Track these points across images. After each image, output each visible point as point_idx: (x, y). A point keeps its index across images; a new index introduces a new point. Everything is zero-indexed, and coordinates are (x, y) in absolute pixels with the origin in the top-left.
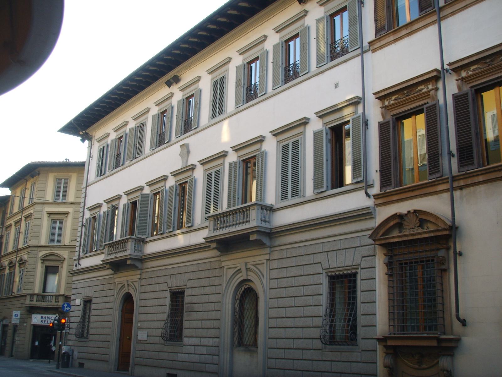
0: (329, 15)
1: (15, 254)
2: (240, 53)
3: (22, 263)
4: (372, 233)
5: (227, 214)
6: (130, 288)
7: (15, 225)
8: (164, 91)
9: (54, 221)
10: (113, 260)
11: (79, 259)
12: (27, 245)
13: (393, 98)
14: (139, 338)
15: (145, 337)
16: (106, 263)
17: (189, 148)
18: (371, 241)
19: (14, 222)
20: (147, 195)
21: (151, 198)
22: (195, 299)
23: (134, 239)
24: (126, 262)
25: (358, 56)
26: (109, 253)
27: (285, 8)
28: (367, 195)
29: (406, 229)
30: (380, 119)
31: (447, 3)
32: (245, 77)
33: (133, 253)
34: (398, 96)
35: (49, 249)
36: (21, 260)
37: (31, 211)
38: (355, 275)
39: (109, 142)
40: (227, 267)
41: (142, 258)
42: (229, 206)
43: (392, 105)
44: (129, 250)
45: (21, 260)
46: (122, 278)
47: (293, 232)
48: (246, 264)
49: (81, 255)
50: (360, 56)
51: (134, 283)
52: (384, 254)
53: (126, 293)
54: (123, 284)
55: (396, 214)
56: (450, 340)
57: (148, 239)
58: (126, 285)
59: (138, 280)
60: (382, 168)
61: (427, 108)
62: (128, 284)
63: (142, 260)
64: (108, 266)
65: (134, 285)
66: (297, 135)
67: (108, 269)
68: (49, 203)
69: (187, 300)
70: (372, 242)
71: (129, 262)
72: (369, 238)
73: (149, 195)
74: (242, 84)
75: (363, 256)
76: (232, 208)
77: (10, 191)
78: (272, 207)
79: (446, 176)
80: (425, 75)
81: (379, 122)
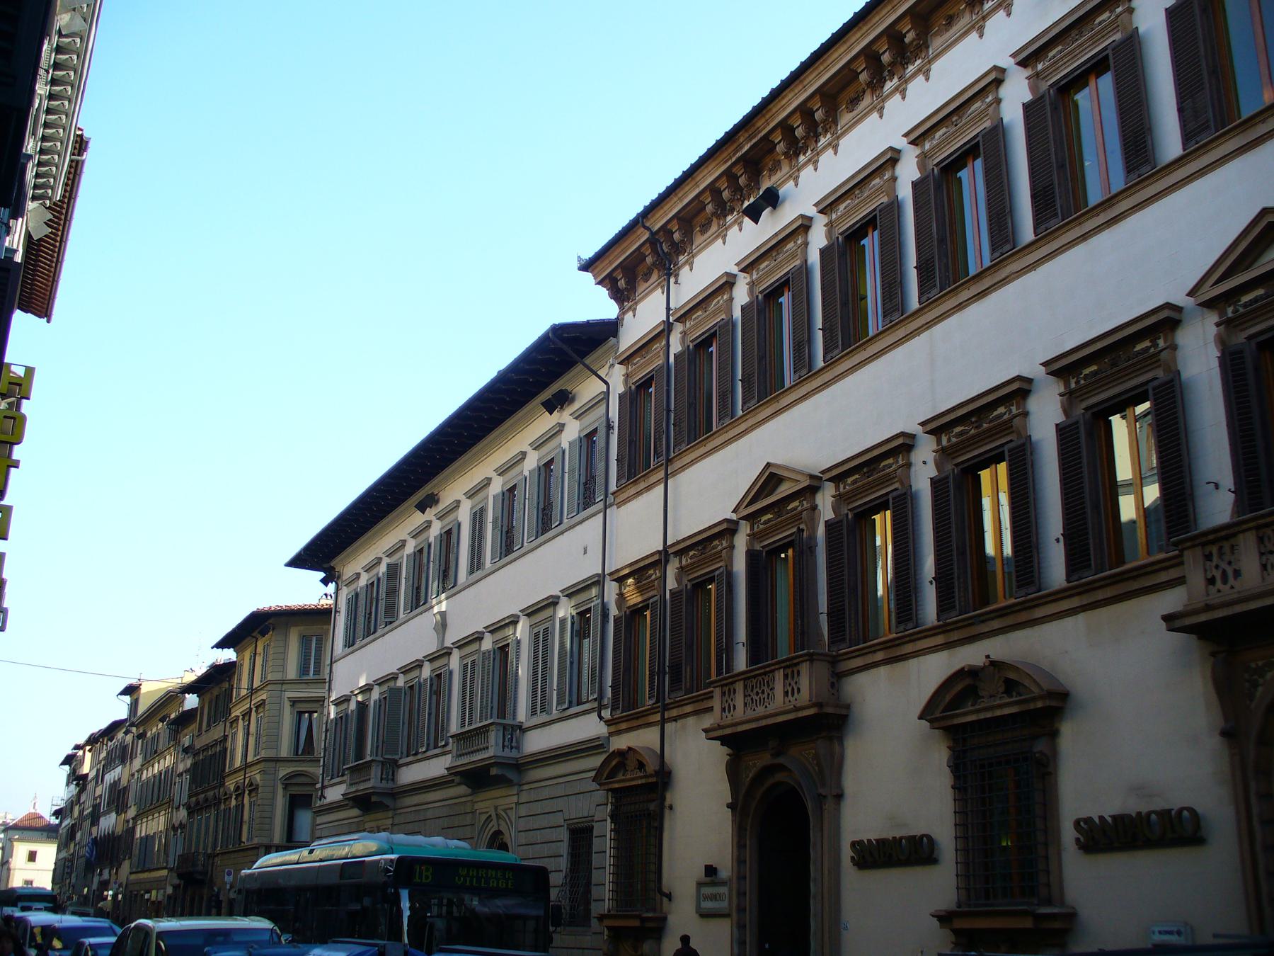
0: (507, 490)
1: (242, 772)
2: (534, 447)
3: (253, 788)
4: (597, 773)
6: (502, 822)
7: (256, 711)
8: (544, 422)
9: (300, 714)
10: (354, 795)
11: (323, 787)
12: (258, 757)
13: (850, 480)
16: (455, 774)
17: (446, 617)
18: (594, 786)
19: (241, 713)
20: (399, 689)
21: (405, 694)
23: (379, 761)
24: (371, 799)
25: (598, 512)
26: (458, 753)
27: (525, 426)
28: (601, 718)
29: (983, 697)
30: (1060, 418)
31: (1039, 236)
33: (500, 753)
34: (962, 428)
35: (296, 764)
36: (251, 784)
37: (264, 697)
38: (591, 829)
39: (565, 445)
40: (481, 811)
41: (517, 761)
42: (463, 725)
43: (1244, 315)
44: (493, 748)
45: (251, 784)
47: (573, 757)
48: (496, 808)
50: (602, 513)
51: (508, 811)
52: (948, 747)
53: (495, 831)
54: (489, 814)
55: (962, 670)
56: (1053, 917)
57: (401, 762)
58: (494, 817)
59: (390, 826)
60: (1068, 530)
61: (1154, 389)
62: (497, 814)
63: (521, 766)
64: (457, 779)
65: (508, 816)
67: (459, 784)
68: (292, 682)
70: (598, 787)
71: (494, 771)
72: (593, 781)
73: (401, 689)
74: (500, 526)
76: (467, 728)
77: (235, 654)
78: (521, 726)
79: (1045, 590)
80: (835, 468)
81: (1057, 425)
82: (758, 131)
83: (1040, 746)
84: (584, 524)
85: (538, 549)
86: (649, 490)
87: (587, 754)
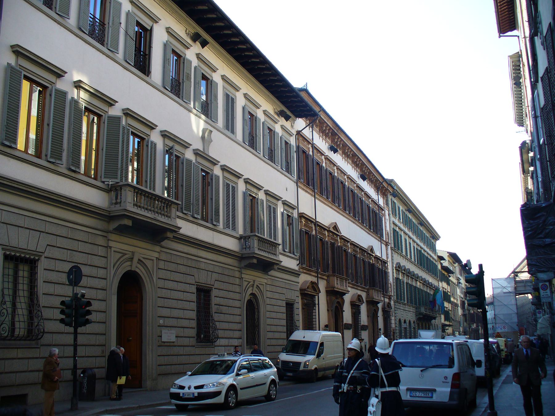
5: (153, 197)
10: (150, 221)
14: (164, 339)
15: (173, 339)
22: (222, 302)
32: (109, 11)
46: (250, 276)
49: (191, 214)
66: (45, 80)
69: (214, 301)
75: (49, 244)
82: (340, 133)
83: (354, 310)
84: (286, 177)
85: (267, 164)
86: (305, 192)
87: (178, 241)
